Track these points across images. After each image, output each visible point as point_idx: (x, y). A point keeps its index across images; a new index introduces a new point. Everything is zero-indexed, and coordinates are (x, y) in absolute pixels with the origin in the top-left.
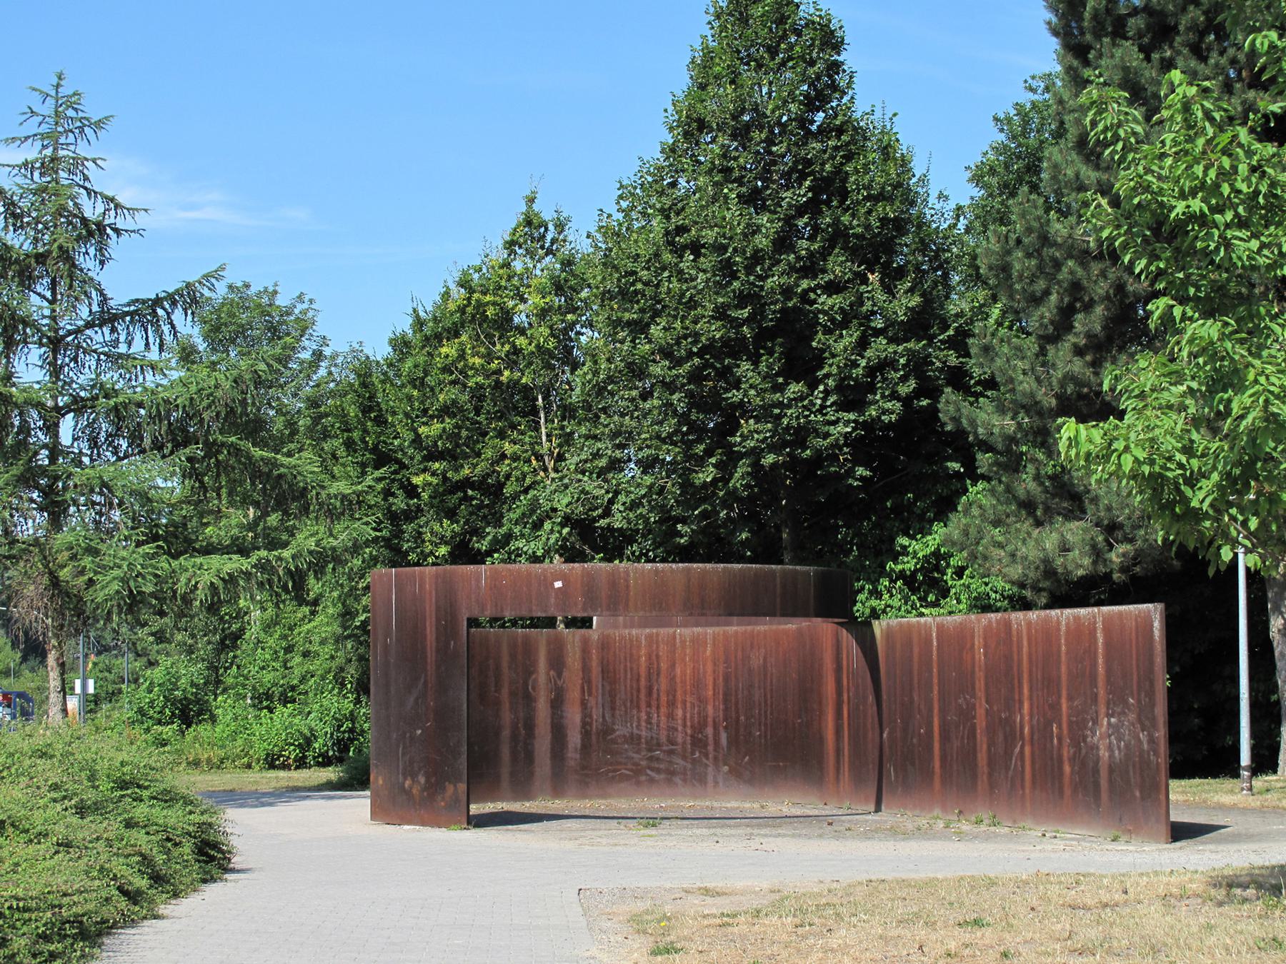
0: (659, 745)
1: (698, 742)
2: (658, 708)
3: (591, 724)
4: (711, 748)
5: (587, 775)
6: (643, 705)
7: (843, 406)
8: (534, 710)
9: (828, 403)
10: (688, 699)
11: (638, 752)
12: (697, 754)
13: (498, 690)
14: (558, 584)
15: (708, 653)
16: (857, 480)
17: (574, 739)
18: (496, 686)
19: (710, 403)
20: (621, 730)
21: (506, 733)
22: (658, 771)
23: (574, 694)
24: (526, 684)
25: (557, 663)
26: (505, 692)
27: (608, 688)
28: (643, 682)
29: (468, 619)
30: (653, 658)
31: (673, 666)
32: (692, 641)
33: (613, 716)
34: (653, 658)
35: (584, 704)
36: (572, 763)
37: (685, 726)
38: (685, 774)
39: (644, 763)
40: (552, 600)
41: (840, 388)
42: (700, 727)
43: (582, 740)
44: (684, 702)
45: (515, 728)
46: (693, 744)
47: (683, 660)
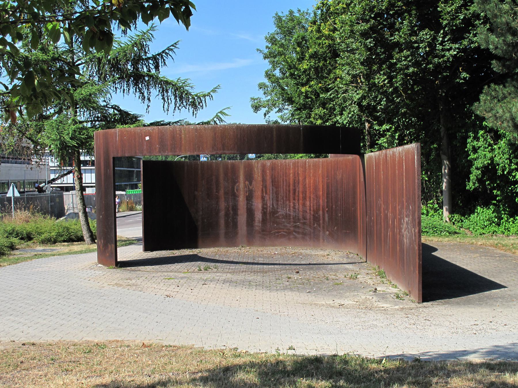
0: (299, 219)
1: (316, 219)
2: (298, 200)
3: (266, 209)
4: (321, 222)
5: (264, 235)
6: (291, 198)
7: (454, 40)
8: (237, 201)
9: (446, 40)
10: (312, 196)
11: (289, 223)
12: (316, 225)
13: (218, 191)
14: (147, 138)
15: (320, 172)
16: (461, 79)
17: (258, 216)
18: (217, 189)
19: (381, 41)
20: (281, 212)
21: (222, 213)
22: (298, 233)
23: (258, 193)
24: (233, 188)
25: (249, 177)
26: (222, 192)
27: (275, 190)
28: (291, 187)
29: (114, 158)
30: (296, 175)
31: (305, 179)
32: (313, 166)
33: (277, 204)
34: (296, 175)
35: (263, 198)
36: (257, 228)
37: (310, 210)
38: (310, 235)
39: (292, 229)
40: (145, 147)
41: (452, 32)
42: (316, 211)
43: (262, 216)
44: (310, 198)
45: (227, 209)
46: (314, 220)
47: (310, 176)
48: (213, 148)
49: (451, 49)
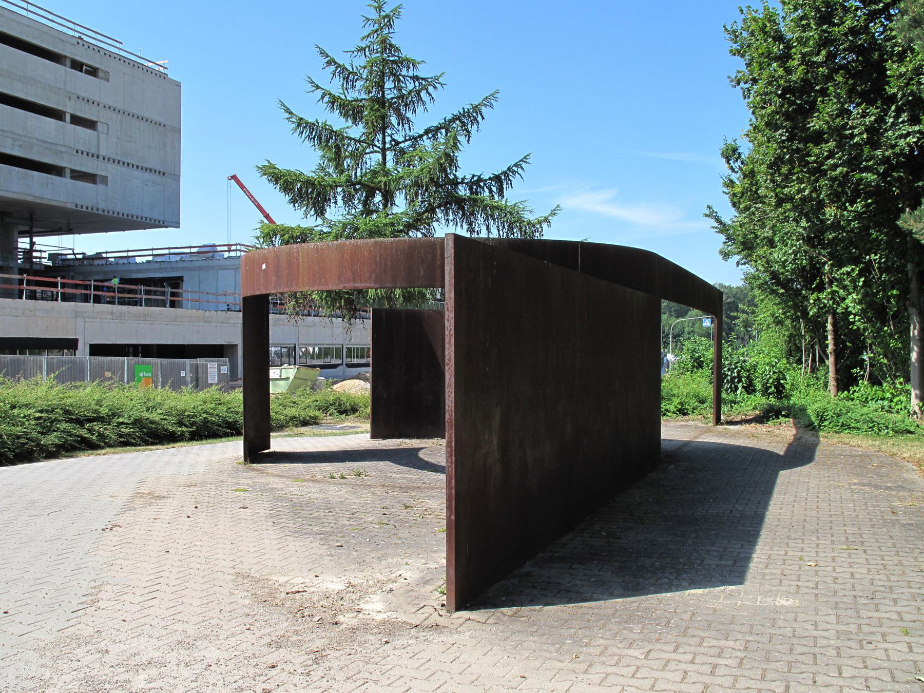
9: (900, 120)
48: (339, 279)
49: (908, 134)
